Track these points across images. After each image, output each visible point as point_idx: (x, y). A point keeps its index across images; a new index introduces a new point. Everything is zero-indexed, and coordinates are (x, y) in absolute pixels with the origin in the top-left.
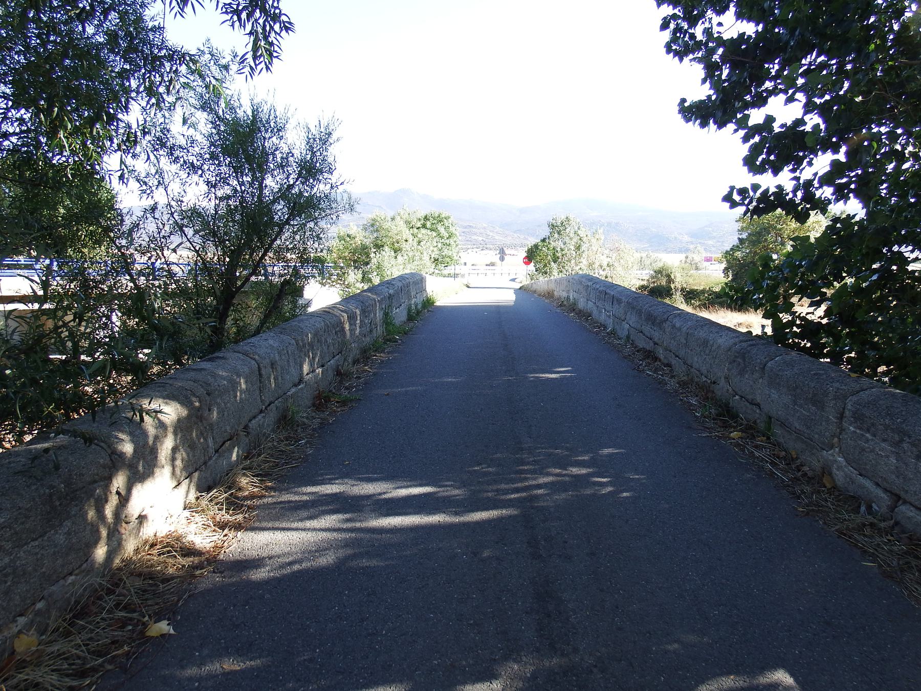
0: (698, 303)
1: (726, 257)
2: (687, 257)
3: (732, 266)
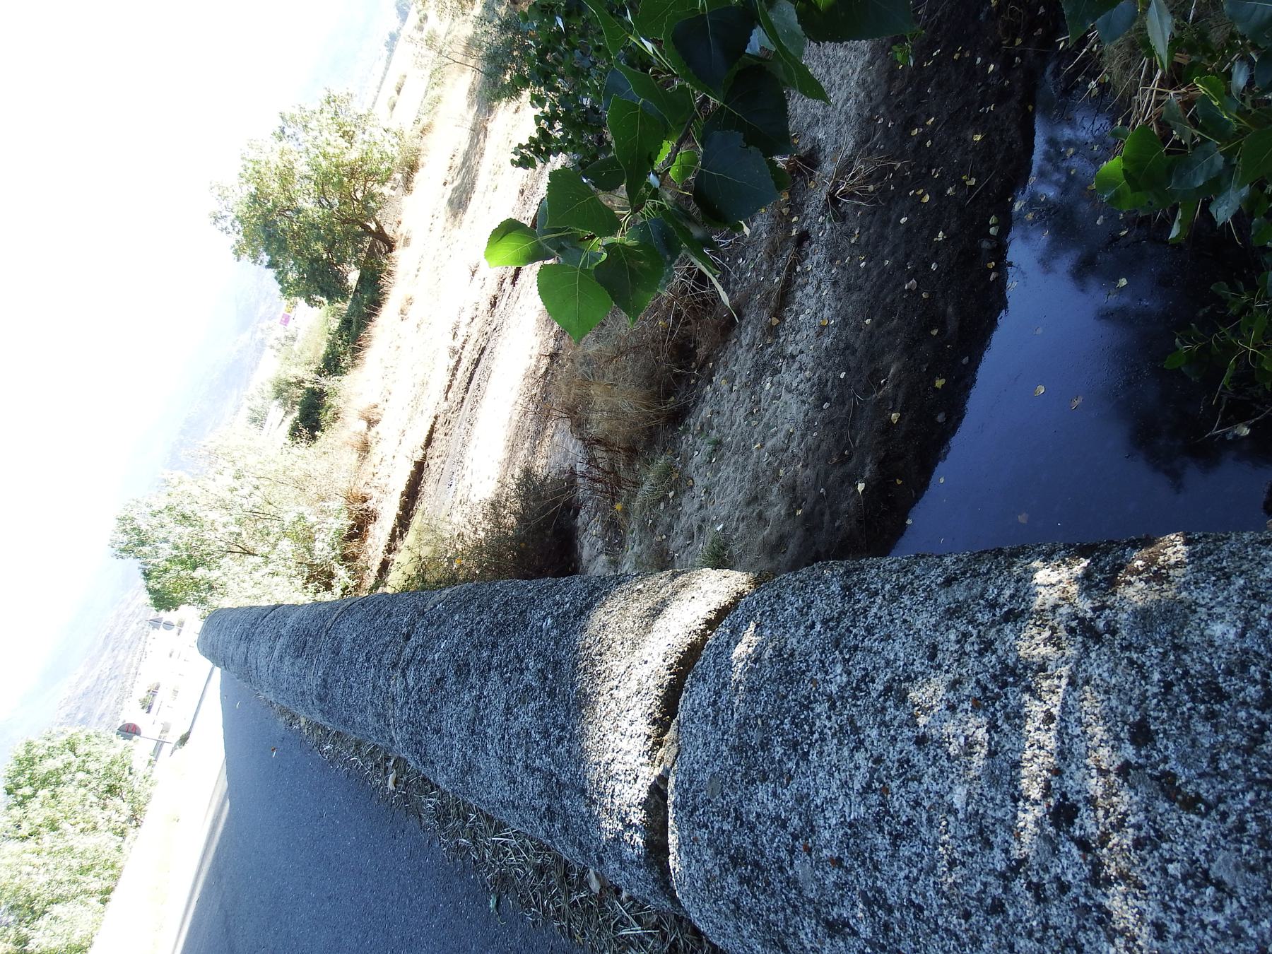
0: (348, 358)
1: (290, 295)
2: (272, 347)
3: (307, 291)
